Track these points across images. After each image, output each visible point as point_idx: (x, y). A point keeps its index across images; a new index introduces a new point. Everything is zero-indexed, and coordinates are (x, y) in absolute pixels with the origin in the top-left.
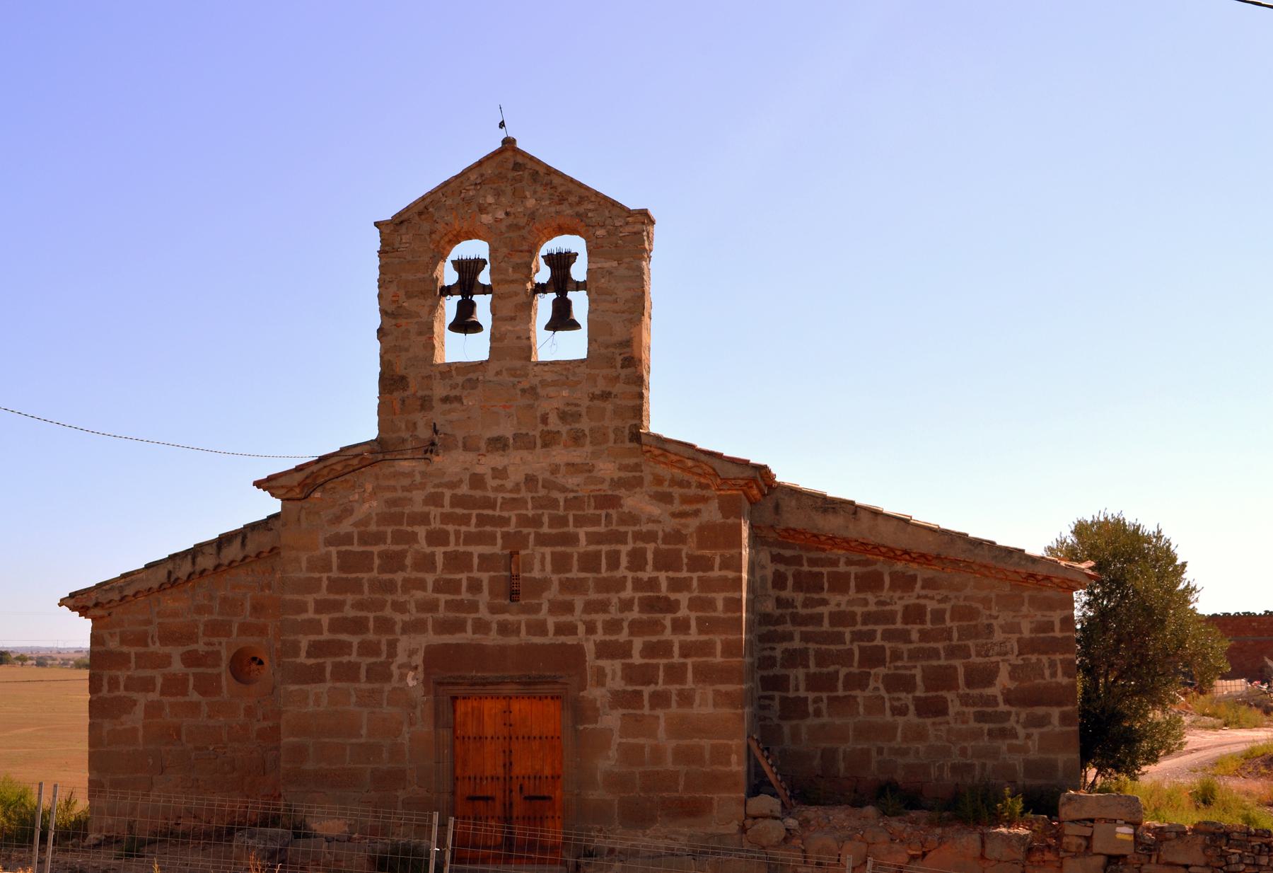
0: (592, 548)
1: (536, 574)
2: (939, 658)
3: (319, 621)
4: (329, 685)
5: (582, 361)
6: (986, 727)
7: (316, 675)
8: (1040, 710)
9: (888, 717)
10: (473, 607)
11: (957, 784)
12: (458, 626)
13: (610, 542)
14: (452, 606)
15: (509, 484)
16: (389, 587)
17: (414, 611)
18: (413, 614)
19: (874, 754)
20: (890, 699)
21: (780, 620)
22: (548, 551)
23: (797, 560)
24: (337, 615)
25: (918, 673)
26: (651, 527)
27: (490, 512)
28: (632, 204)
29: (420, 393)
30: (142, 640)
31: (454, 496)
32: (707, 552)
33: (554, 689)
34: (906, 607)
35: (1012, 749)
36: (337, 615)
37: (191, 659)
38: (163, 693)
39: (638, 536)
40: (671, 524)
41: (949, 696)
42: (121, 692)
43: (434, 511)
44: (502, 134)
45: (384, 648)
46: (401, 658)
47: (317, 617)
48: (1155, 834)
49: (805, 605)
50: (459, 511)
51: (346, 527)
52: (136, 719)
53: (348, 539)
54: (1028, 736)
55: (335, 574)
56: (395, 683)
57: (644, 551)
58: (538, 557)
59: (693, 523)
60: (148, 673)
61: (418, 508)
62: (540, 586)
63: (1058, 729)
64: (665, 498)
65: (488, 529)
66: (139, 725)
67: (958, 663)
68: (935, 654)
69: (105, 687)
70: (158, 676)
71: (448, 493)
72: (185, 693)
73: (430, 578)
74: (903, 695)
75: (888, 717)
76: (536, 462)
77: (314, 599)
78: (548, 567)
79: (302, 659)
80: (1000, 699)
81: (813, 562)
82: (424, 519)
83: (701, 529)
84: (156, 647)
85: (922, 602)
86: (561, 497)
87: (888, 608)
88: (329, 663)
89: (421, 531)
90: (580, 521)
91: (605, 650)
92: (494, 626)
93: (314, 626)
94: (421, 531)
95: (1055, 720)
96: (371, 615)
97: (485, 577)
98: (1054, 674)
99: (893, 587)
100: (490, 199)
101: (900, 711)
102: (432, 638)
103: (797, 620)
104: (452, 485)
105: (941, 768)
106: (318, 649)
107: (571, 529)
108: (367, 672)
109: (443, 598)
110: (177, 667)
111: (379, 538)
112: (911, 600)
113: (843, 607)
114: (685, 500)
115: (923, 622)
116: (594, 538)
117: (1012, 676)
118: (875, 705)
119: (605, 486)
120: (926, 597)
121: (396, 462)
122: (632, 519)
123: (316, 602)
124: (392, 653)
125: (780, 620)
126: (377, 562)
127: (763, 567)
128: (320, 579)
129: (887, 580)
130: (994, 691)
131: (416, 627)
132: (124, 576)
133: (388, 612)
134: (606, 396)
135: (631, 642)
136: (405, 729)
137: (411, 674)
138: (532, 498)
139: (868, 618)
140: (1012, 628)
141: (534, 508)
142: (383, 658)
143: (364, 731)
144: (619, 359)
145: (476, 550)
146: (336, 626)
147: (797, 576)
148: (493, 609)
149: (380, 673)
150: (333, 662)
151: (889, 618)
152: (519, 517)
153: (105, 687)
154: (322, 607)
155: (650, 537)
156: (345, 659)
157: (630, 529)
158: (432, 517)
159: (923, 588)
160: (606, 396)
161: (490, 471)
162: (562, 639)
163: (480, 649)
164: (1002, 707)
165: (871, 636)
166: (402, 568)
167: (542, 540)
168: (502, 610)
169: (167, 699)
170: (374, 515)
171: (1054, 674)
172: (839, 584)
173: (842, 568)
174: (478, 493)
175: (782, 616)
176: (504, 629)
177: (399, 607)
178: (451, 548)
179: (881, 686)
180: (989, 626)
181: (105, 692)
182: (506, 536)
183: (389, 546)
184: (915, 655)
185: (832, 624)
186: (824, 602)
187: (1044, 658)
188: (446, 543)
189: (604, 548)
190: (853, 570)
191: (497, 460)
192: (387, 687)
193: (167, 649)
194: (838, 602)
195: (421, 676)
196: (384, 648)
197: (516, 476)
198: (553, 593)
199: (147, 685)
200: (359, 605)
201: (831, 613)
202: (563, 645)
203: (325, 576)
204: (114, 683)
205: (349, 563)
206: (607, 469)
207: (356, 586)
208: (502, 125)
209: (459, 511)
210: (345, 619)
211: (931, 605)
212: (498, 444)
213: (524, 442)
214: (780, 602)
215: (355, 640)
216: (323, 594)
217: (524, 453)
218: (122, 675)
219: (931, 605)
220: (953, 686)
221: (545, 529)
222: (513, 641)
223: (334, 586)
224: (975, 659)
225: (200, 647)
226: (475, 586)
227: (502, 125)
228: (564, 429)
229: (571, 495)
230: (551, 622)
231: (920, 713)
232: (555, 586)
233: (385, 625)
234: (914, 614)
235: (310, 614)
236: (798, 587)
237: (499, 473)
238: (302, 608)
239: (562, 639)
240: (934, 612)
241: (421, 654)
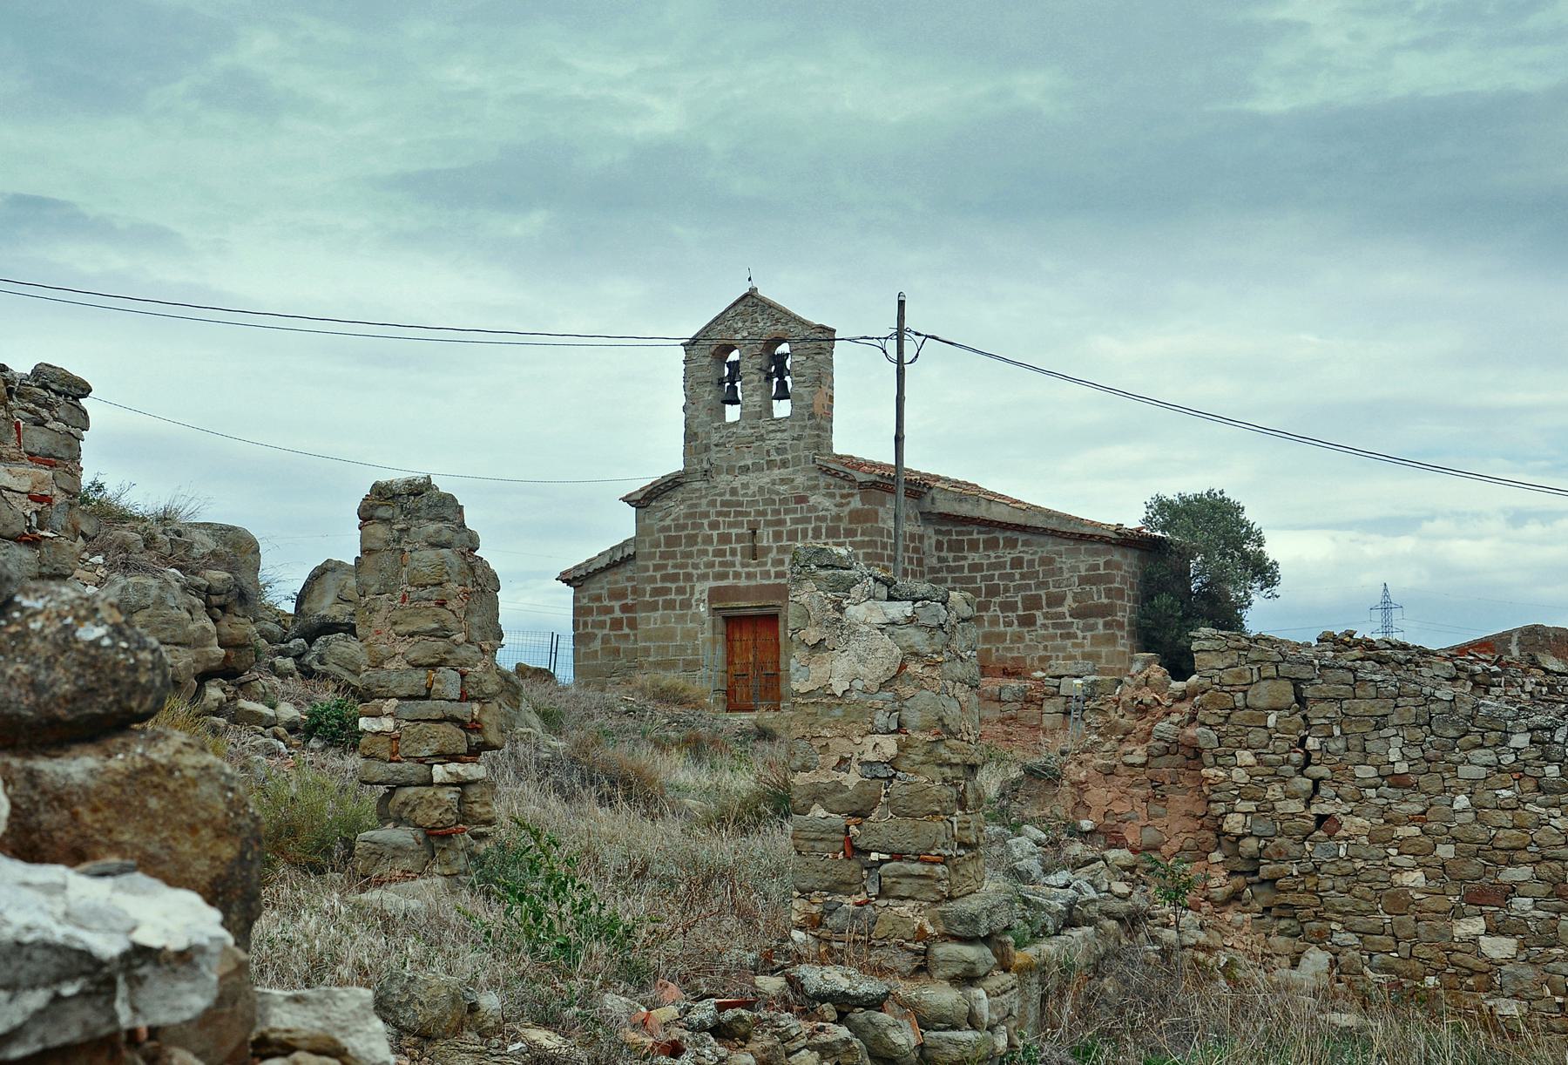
0: (793, 527)
1: (765, 543)
2: (1031, 590)
4: (660, 612)
5: (787, 418)
6: (1059, 632)
7: (653, 607)
8: (1092, 621)
9: (1002, 628)
10: (733, 564)
12: (724, 576)
13: (802, 523)
14: (722, 564)
15: (750, 492)
16: (689, 555)
18: (702, 570)
19: (994, 651)
20: (1004, 617)
21: (940, 570)
23: (949, 533)
24: (664, 572)
25: (1019, 599)
26: (824, 513)
27: (740, 509)
30: (598, 598)
31: (721, 501)
32: (854, 526)
33: (739, 608)
34: (1013, 558)
35: (1075, 645)
36: (664, 572)
37: (625, 608)
38: (610, 630)
39: (818, 519)
40: (834, 510)
41: (1038, 613)
42: (589, 630)
43: (712, 511)
44: (749, 285)
45: (688, 590)
46: (697, 596)
49: (954, 561)
50: (725, 509)
51: (668, 522)
52: (597, 645)
53: (668, 528)
54: (1084, 638)
55: (663, 549)
56: (694, 609)
57: (820, 527)
59: (847, 510)
60: (602, 618)
61: (704, 508)
62: (768, 550)
63: (1102, 632)
64: (832, 496)
65: (740, 519)
66: (599, 648)
67: (1042, 593)
68: (1028, 587)
69: (581, 628)
70: (607, 618)
71: (719, 499)
72: (621, 629)
73: (710, 549)
74: (1010, 614)
75: (1002, 628)
76: (764, 479)
78: (771, 540)
79: (647, 598)
80: (1067, 615)
81: (958, 533)
82: (706, 515)
83: (851, 512)
84: (606, 603)
85: (1021, 555)
86: (777, 498)
87: (1002, 560)
88: (660, 599)
89: (706, 522)
90: (787, 512)
93: (652, 579)
94: (706, 522)
95: (1101, 627)
96: (681, 572)
97: (738, 546)
98: (1100, 597)
99: (1005, 546)
100: (740, 325)
101: (1010, 624)
103: (950, 570)
104: (721, 495)
105: (1032, 659)
106: (657, 592)
109: (718, 560)
110: (618, 614)
111: (684, 527)
112: (1015, 553)
113: (976, 561)
114: (842, 496)
115: (1022, 568)
116: (795, 521)
117: (1074, 601)
118: (994, 621)
119: (800, 491)
120: (1023, 552)
122: (813, 509)
123: (654, 565)
124: (692, 594)
125: (940, 570)
127: (930, 538)
129: (1001, 542)
130: (1064, 609)
131: (704, 577)
132: (588, 561)
133: (690, 570)
134: (799, 438)
136: (699, 636)
139: (991, 566)
140: (1074, 569)
141: (764, 505)
144: (807, 415)
145: (734, 531)
146: (665, 578)
147: (949, 541)
148: (743, 565)
149: (686, 605)
151: (1002, 566)
152: (755, 511)
153: (581, 628)
154: (657, 568)
155: (823, 519)
156: (668, 597)
157: (813, 515)
159: (1022, 546)
160: (799, 438)
161: (740, 486)
162: (778, 581)
163: (735, 588)
164: (1069, 619)
165: (992, 577)
166: (696, 544)
167: (768, 524)
168: (748, 565)
169: (611, 633)
171: (1100, 597)
172: (974, 546)
173: (975, 536)
174: (734, 498)
175: (941, 567)
176: (749, 576)
177: (696, 566)
178: (721, 531)
179: (998, 609)
180: (1061, 568)
181: (581, 630)
182: (749, 522)
183: (689, 531)
184: (1018, 588)
185: (970, 572)
186: (965, 558)
187: (1094, 588)
188: (719, 529)
189: (800, 526)
190: (982, 537)
191: (744, 478)
192: (690, 612)
193: (612, 603)
194: (973, 557)
196: (688, 590)
197: (753, 489)
198: (773, 554)
199: (602, 625)
201: (969, 565)
204: (585, 624)
205: (671, 542)
206: (800, 479)
207: (673, 556)
208: (750, 279)
209: (725, 509)
211: (1027, 557)
212: (745, 470)
213: (758, 468)
214: (940, 559)
215: (674, 586)
216: (657, 561)
217: (757, 473)
218: (590, 619)
219: (1027, 557)
220: (1039, 608)
221: (769, 517)
222: (753, 583)
223: (663, 556)
224: (1052, 590)
225: (629, 601)
226: (733, 552)
227: (750, 279)
228: (778, 458)
230: (773, 571)
231: (1020, 625)
232: (775, 550)
233: (688, 577)
234: (1018, 562)
235: (651, 573)
236: (950, 549)
237: (745, 486)
238: (646, 569)
239: (778, 581)
240: (1029, 561)
241: (707, 592)
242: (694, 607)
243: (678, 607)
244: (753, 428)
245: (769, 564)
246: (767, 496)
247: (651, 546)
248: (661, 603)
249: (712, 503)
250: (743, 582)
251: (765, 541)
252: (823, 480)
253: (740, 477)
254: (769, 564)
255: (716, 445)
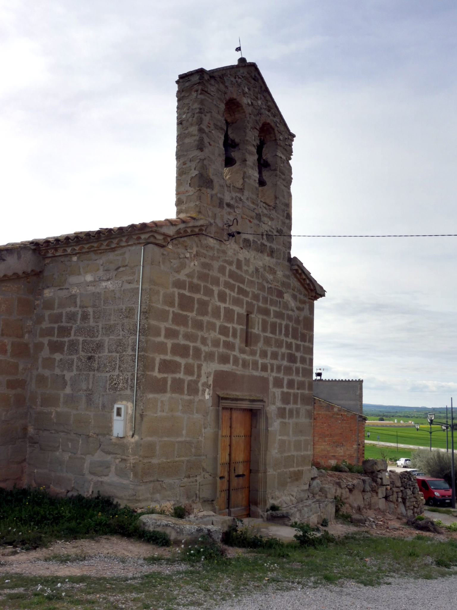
0: (275, 320)
3: (166, 344)
11: (194, 403)
17: (210, 344)
22: (261, 317)
28: (292, 130)
29: (219, 195)
36: (176, 341)
45: (196, 370)
46: (203, 379)
47: (165, 341)
48: (180, 530)
50: (232, 282)
51: (182, 276)
56: (200, 397)
58: (257, 320)
65: (241, 297)
71: (228, 268)
77: (165, 327)
79: (156, 374)
88: (170, 377)
91: (278, 383)
92: (241, 361)
93: (161, 348)
94: (216, 289)
102: (215, 366)
106: (166, 366)
107: (268, 306)
108: (188, 385)
109: (223, 338)
121: (208, 238)
124: (199, 376)
126: (196, 306)
128: (169, 311)
131: (210, 357)
133: (198, 344)
135: (283, 378)
136: (203, 430)
137: (207, 390)
138: (257, 282)
142: (195, 378)
143: (184, 432)
148: (242, 351)
149: (193, 389)
150: (172, 378)
158: (221, 281)
170: (196, 271)
177: (204, 341)
182: (247, 302)
192: (197, 399)
195: (211, 392)
196: (196, 370)
200: (187, 336)
202: (263, 377)
203: (171, 310)
210: (178, 345)
215: (182, 361)
216: (169, 324)
229: (270, 286)
233: (197, 352)
235: (162, 339)
237: (247, 261)
242: (200, 393)
243: (186, 392)
244: (253, 203)
245: (258, 355)
246: (260, 281)
247: (165, 302)
248: (169, 382)
249: (222, 270)
250: (239, 370)
251: (256, 328)
252: (294, 282)
253: (244, 250)
254: (258, 355)
255: (228, 205)
